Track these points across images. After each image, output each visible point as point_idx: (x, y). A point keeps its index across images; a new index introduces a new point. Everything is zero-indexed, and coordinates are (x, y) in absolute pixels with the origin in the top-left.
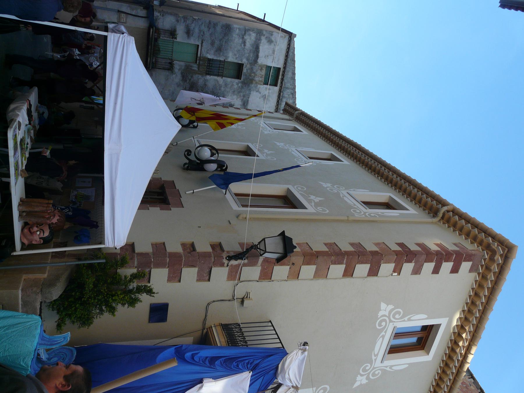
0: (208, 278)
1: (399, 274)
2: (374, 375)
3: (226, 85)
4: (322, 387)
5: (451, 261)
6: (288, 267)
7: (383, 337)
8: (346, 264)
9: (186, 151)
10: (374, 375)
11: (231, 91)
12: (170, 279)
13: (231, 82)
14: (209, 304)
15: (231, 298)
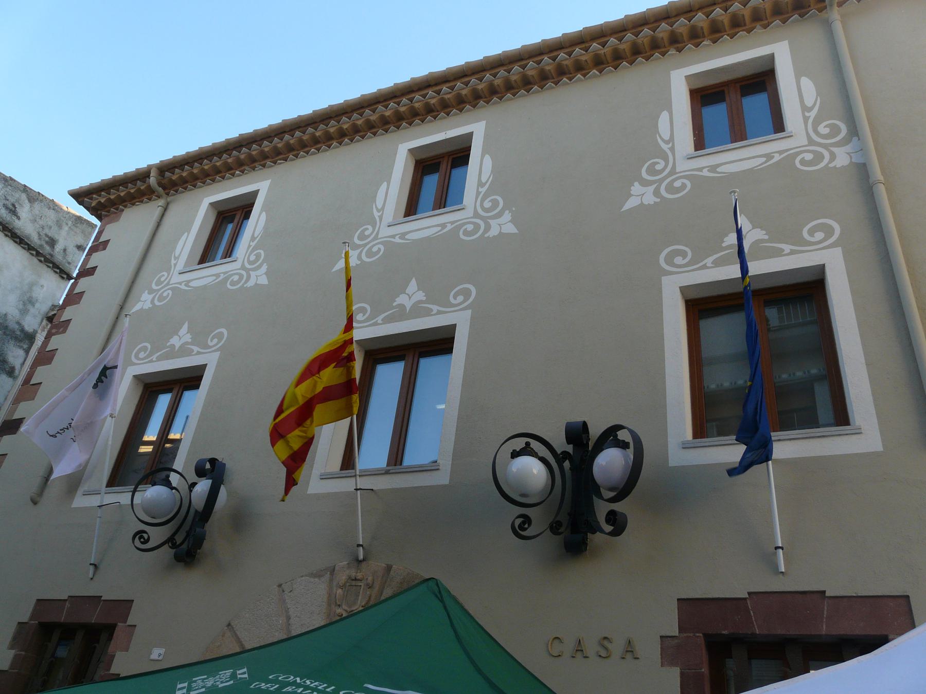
4: (461, 287)
10: (670, 189)
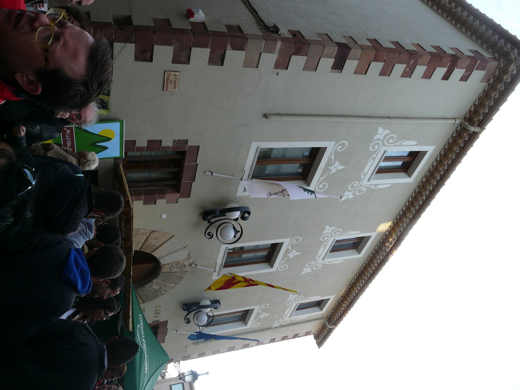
2: (360, 191)
7: (325, 245)
10: (360, 191)
12: (212, 61)
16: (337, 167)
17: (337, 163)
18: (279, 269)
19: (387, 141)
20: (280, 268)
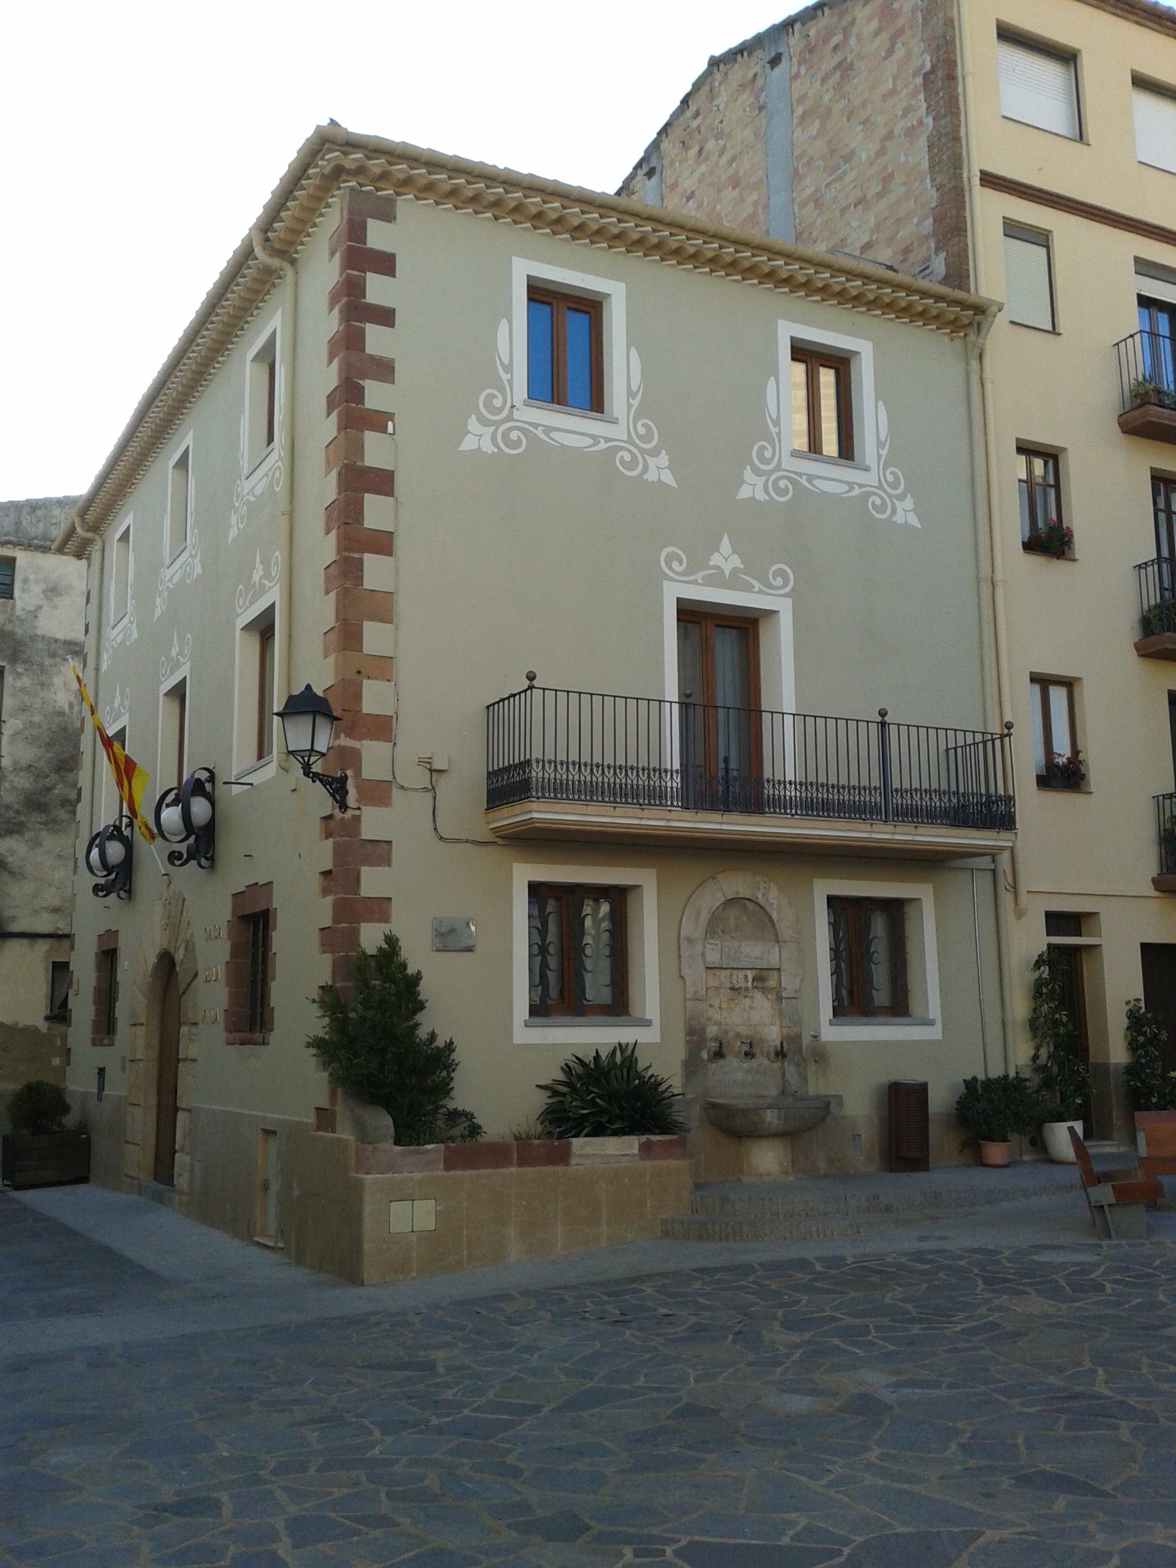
0: (384, 845)
1: (390, 416)
3: (24, 709)
5: (364, 279)
6: (366, 683)
8: (362, 551)
9: (173, 864)
10: (894, 486)
11: (42, 695)
13: (13, 695)
14: (441, 838)
15: (430, 795)
16: (725, 558)
17: (716, 559)
18: (788, 589)
19: (499, 411)
20: (785, 585)
